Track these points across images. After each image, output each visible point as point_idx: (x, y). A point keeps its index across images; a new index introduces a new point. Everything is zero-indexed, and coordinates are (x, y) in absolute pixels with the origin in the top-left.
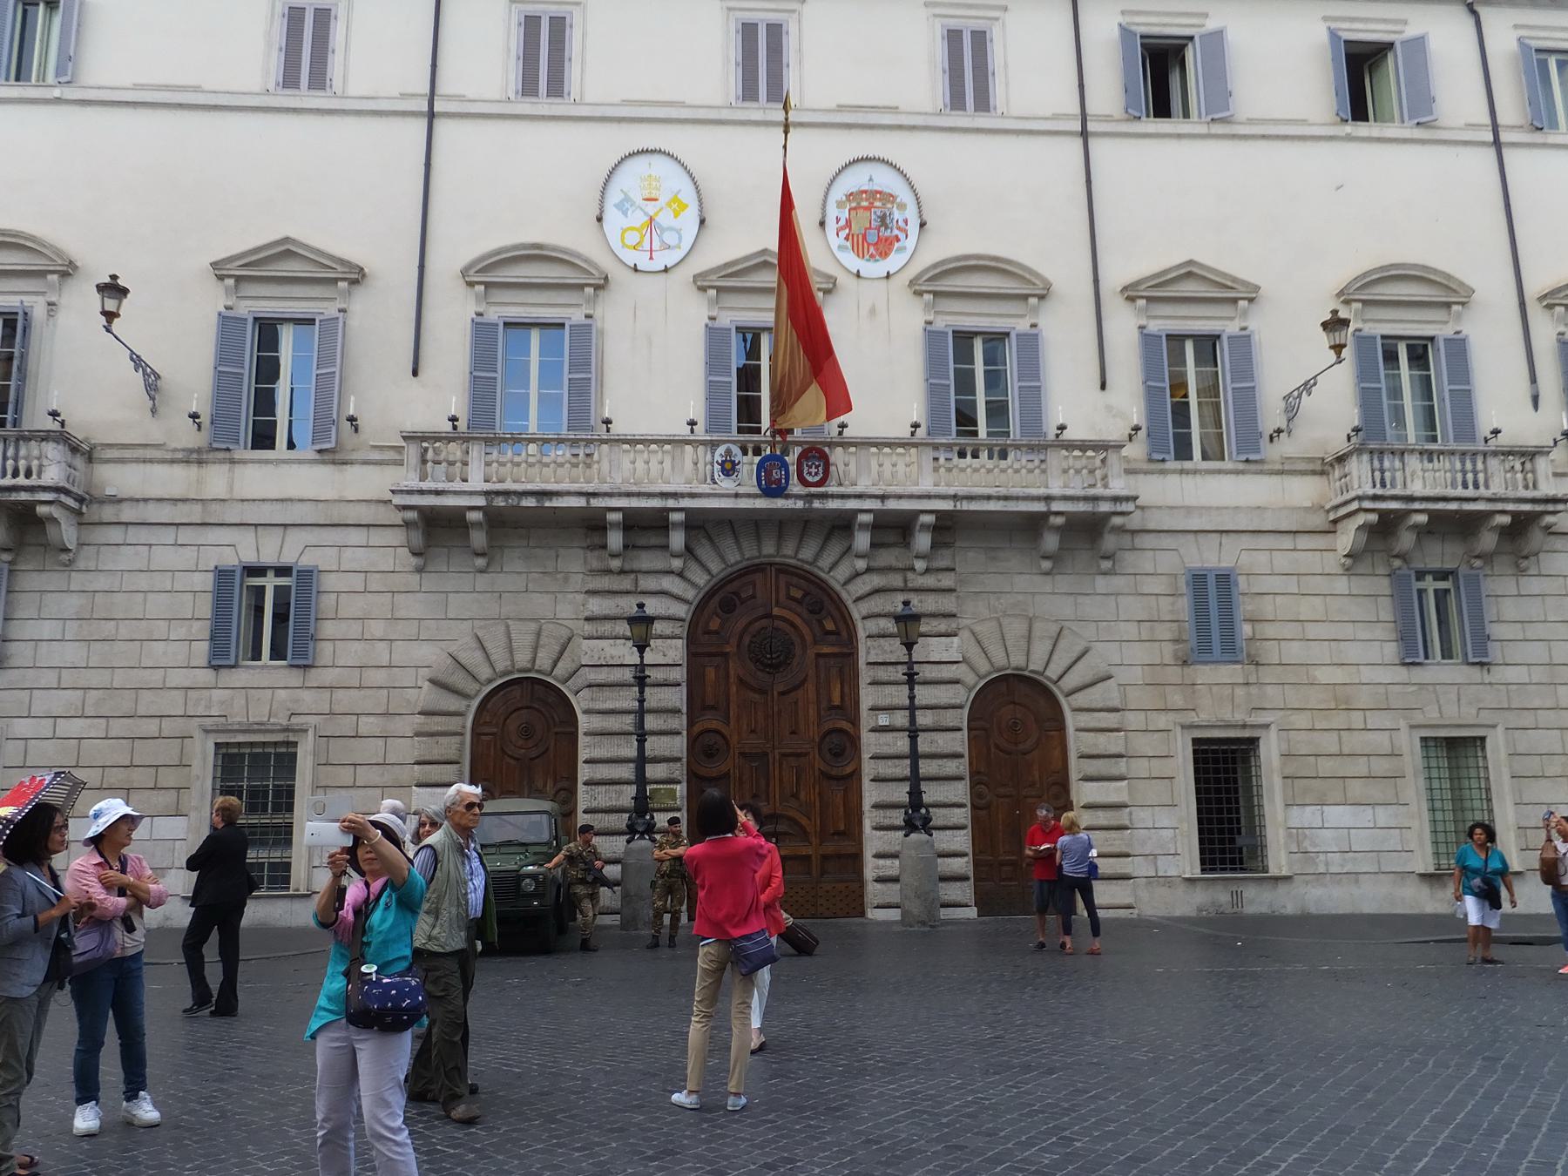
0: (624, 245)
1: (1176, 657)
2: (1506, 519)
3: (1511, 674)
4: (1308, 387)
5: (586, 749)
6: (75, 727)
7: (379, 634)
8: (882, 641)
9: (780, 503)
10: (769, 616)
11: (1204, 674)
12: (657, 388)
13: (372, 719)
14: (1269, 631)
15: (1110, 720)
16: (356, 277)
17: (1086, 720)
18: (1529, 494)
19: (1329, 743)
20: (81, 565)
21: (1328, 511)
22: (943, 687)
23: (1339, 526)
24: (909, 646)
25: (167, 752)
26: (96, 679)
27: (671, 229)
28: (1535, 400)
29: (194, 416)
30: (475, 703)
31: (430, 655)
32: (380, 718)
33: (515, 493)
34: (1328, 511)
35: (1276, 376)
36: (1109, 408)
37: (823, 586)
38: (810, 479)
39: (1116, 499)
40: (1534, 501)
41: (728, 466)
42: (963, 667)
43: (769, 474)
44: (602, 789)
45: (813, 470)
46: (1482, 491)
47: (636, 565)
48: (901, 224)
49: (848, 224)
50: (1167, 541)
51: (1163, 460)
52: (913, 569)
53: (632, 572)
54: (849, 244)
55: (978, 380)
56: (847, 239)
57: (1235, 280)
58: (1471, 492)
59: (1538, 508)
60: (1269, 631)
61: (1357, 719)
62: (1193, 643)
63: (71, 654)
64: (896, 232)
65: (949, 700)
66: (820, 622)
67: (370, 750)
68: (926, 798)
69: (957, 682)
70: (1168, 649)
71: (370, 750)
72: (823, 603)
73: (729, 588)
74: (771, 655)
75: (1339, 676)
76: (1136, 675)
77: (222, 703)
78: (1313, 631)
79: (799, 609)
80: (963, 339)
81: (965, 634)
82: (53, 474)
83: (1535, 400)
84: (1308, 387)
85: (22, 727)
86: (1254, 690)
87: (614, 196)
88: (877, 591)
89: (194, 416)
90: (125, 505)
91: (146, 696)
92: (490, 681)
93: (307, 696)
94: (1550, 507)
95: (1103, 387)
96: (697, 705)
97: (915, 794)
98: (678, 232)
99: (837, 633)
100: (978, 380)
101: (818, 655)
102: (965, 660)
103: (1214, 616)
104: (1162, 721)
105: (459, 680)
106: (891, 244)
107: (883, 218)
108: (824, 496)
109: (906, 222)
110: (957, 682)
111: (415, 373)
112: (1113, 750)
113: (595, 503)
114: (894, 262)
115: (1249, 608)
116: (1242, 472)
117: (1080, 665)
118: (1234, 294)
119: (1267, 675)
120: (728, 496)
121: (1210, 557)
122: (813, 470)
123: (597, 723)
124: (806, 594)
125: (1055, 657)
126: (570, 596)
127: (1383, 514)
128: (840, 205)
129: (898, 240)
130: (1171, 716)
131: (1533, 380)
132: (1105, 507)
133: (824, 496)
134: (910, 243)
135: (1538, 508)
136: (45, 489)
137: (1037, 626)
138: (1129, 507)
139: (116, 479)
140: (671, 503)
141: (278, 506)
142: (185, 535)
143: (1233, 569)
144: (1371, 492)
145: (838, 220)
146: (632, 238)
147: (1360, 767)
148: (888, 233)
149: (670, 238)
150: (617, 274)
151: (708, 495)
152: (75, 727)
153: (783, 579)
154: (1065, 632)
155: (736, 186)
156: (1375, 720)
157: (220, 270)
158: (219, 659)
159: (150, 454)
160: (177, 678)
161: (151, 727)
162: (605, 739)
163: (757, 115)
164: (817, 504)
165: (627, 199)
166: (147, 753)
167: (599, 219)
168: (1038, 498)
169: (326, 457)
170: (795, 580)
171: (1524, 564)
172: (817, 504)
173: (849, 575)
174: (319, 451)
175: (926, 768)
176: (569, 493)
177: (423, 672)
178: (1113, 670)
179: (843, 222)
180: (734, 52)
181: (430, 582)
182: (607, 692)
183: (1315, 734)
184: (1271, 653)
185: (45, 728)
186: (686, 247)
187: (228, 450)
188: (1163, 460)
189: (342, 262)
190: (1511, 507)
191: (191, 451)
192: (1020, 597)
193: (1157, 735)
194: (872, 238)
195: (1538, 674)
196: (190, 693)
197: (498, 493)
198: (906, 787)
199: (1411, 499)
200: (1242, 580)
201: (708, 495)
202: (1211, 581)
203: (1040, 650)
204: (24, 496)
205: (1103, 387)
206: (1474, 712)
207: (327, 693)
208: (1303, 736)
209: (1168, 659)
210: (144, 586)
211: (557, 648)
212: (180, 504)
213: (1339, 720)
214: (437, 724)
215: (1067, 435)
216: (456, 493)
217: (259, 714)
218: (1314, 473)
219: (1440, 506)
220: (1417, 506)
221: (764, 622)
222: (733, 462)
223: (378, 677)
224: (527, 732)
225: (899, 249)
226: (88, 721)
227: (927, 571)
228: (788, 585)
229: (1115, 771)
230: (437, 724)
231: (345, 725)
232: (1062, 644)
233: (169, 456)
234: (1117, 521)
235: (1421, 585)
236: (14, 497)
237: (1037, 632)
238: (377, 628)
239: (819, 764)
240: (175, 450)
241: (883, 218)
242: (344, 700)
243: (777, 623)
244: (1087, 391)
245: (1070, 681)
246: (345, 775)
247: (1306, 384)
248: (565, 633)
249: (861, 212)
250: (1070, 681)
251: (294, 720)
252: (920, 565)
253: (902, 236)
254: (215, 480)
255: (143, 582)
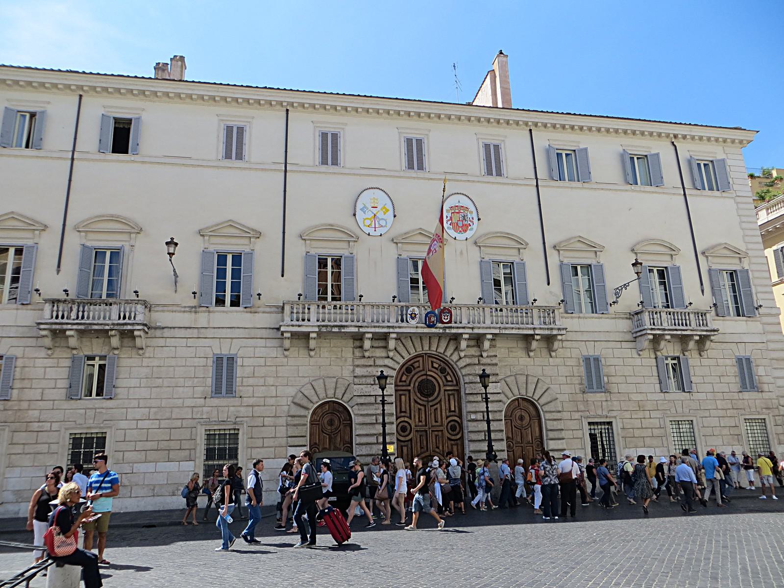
0: (365, 225)
1: (580, 390)
2: (697, 338)
3: (701, 396)
4: (625, 286)
5: (357, 430)
6: (146, 424)
7: (271, 383)
8: (471, 384)
9: (433, 330)
10: (426, 375)
11: (591, 397)
12: (376, 281)
13: (269, 419)
14: (613, 379)
15: (558, 416)
16: (258, 235)
17: (548, 416)
18: (706, 328)
19: (637, 423)
20: (147, 355)
21: (633, 333)
22: (495, 403)
23: (637, 339)
24: (486, 387)
25: (186, 434)
26: (154, 403)
27: (382, 219)
28: (703, 291)
29: (194, 293)
30: (311, 412)
31: (292, 391)
32: (273, 419)
33: (330, 326)
34: (633, 333)
35: (612, 281)
36: (551, 292)
37: (447, 363)
38: (445, 321)
39: (559, 329)
40: (707, 331)
41: (413, 315)
42: (502, 395)
43: (430, 319)
44: (364, 446)
45: (446, 317)
46: (689, 327)
47: (374, 355)
48: (471, 219)
49: (451, 218)
50: (575, 344)
51: (572, 313)
52: (482, 356)
53: (372, 357)
54: (451, 227)
55: (504, 280)
56: (450, 224)
57: (596, 244)
58: (685, 328)
59: (708, 333)
60: (613, 379)
61: (647, 414)
62: (586, 385)
63: (144, 393)
64: (469, 222)
65: (499, 409)
66: (445, 377)
67: (268, 432)
68: (494, 448)
69: (500, 401)
70: (578, 387)
71: (268, 432)
72: (446, 368)
73: (409, 363)
74: (426, 389)
75: (639, 397)
76: (566, 398)
77: (208, 413)
78: (629, 380)
79: (437, 371)
80: (99, 254)
81: (503, 382)
82: (140, 318)
83: (703, 291)
84: (625, 286)
85: (123, 424)
86: (609, 403)
87: (359, 205)
88: (469, 365)
89: (194, 293)
90: (165, 330)
91: (176, 410)
92: (317, 402)
93: (242, 409)
94: (712, 333)
95: (549, 284)
96: (400, 412)
97: (490, 446)
98: (386, 220)
99: (452, 381)
100: (504, 280)
101: (445, 390)
102: (503, 393)
103: (593, 374)
104: (577, 416)
105: (305, 402)
106: (468, 227)
107: (464, 217)
108: (450, 328)
109: (473, 218)
110: (500, 401)
111: (283, 276)
112: (559, 427)
113: (361, 330)
114: (469, 234)
115: (606, 371)
116: (601, 318)
117: (546, 394)
118: (595, 248)
119: (614, 397)
120: (413, 328)
121: (591, 351)
122: (446, 317)
123: (361, 420)
124: (440, 365)
125: (536, 391)
126: (347, 367)
127: (654, 335)
128: (447, 211)
129: (470, 226)
130: (580, 413)
131: (702, 284)
132: (555, 332)
133: (450, 328)
134: (475, 227)
135: (708, 333)
136: (138, 324)
137: (530, 378)
138: (564, 332)
139: (161, 318)
140: (391, 330)
141: (229, 330)
142: (190, 342)
143: (599, 356)
144: (650, 327)
145: (447, 217)
146: (368, 222)
147: (649, 433)
148: (466, 223)
149: (383, 223)
150: (363, 237)
151: (406, 327)
152: (146, 424)
153: (430, 359)
154: (540, 381)
155: (417, 204)
156: (653, 414)
157: (201, 233)
158: (71, 396)
159: (175, 308)
160: (189, 402)
161: (178, 423)
162: (365, 427)
163: (414, 175)
164: (447, 331)
165: (365, 207)
166: (176, 434)
167: (355, 215)
168: (530, 329)
169: (248, 310)
170: (435, 360)
171: (641, 353)
172: (447, 331)
173: (463, 359)
174: (246, 308)
175: (493, 436)
176: (351, 326)
177: (289, 399)
178: (558, 396)
179: (449, 218)
180: (404, 150)
181: (291, 362)
182: (364, 407)
183: (632, 420)
184: (766, 387)
185: (133, 424)
186: (389, 225)
187: (207, 307)
188: (572, 313)
189: (253, 230)
190: (699, 333)
191: (192, 307)
192: (522, 367)
193: (576, 421)
194: (460, 224)
195: (710, 396)
196: (194, 409)
197: (323, 326)
198: (486, 444)
199: (664, 330)
200: (603, 360)
201: (406, 327)
202: (592, 360)
203: (531, 388)
204: (129, 327)
205: (549, 284)
206: (688, 411)
207: (251, 408)
208: (628, 421)
209: (578, 391)
210: (173, 364)
211: (344, 389)
212: (188, 329)
213: (640, 415)
214: (296, 421)
215: (454, 302)
216: (306, 326)
217: (223, 417)
218: (627, 318)
219: (675, 332)
220: (666, 332)
221: (424, 377)
222: (415, 314)
223: (271, 401)
224: (331, 423)
225: (472, 229)
226: (151, 421)
227: (487, 357)
228: (432, 362)
229: (560, 436)
230: (296, 421)
231: (259, 422)
232: (539, 385)
233: (183, 309)
234: (559, 337)
235: (666, 362)
236: (125, 327)
237: (529, 381)
238: (270, 381)
239: (447, 434)
240: (185, 307)
241: (464, 217)
242: (258, 411)
243: (429, 378)
244: (462, 284)
245: (542, 401)
246: (259, 443)
247: (625, 285)
248: (347, 383)
249: (455, 214)
250: (542, 401)
251: (237, 419)
252: (485, 354)
253: (471, 224)
254: (202, 319)
255: (173, 362)
